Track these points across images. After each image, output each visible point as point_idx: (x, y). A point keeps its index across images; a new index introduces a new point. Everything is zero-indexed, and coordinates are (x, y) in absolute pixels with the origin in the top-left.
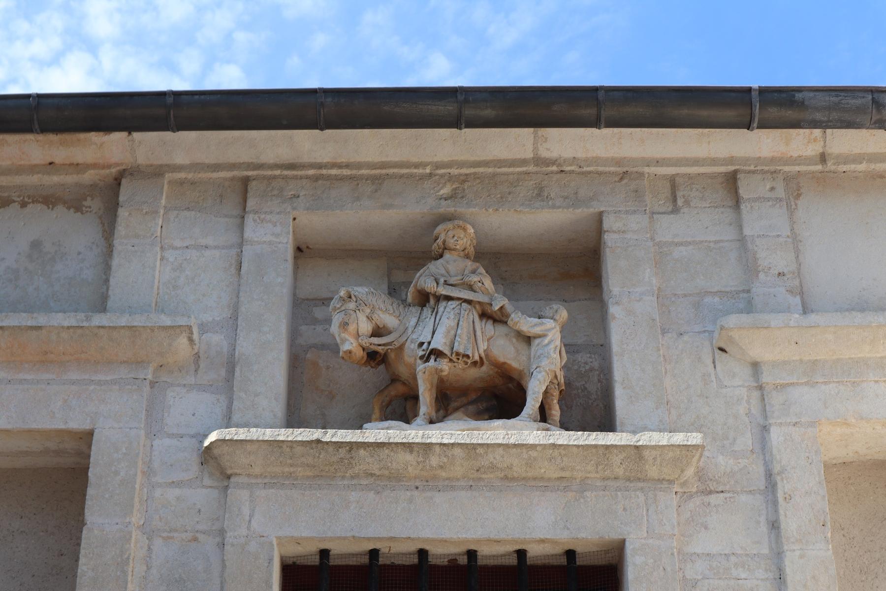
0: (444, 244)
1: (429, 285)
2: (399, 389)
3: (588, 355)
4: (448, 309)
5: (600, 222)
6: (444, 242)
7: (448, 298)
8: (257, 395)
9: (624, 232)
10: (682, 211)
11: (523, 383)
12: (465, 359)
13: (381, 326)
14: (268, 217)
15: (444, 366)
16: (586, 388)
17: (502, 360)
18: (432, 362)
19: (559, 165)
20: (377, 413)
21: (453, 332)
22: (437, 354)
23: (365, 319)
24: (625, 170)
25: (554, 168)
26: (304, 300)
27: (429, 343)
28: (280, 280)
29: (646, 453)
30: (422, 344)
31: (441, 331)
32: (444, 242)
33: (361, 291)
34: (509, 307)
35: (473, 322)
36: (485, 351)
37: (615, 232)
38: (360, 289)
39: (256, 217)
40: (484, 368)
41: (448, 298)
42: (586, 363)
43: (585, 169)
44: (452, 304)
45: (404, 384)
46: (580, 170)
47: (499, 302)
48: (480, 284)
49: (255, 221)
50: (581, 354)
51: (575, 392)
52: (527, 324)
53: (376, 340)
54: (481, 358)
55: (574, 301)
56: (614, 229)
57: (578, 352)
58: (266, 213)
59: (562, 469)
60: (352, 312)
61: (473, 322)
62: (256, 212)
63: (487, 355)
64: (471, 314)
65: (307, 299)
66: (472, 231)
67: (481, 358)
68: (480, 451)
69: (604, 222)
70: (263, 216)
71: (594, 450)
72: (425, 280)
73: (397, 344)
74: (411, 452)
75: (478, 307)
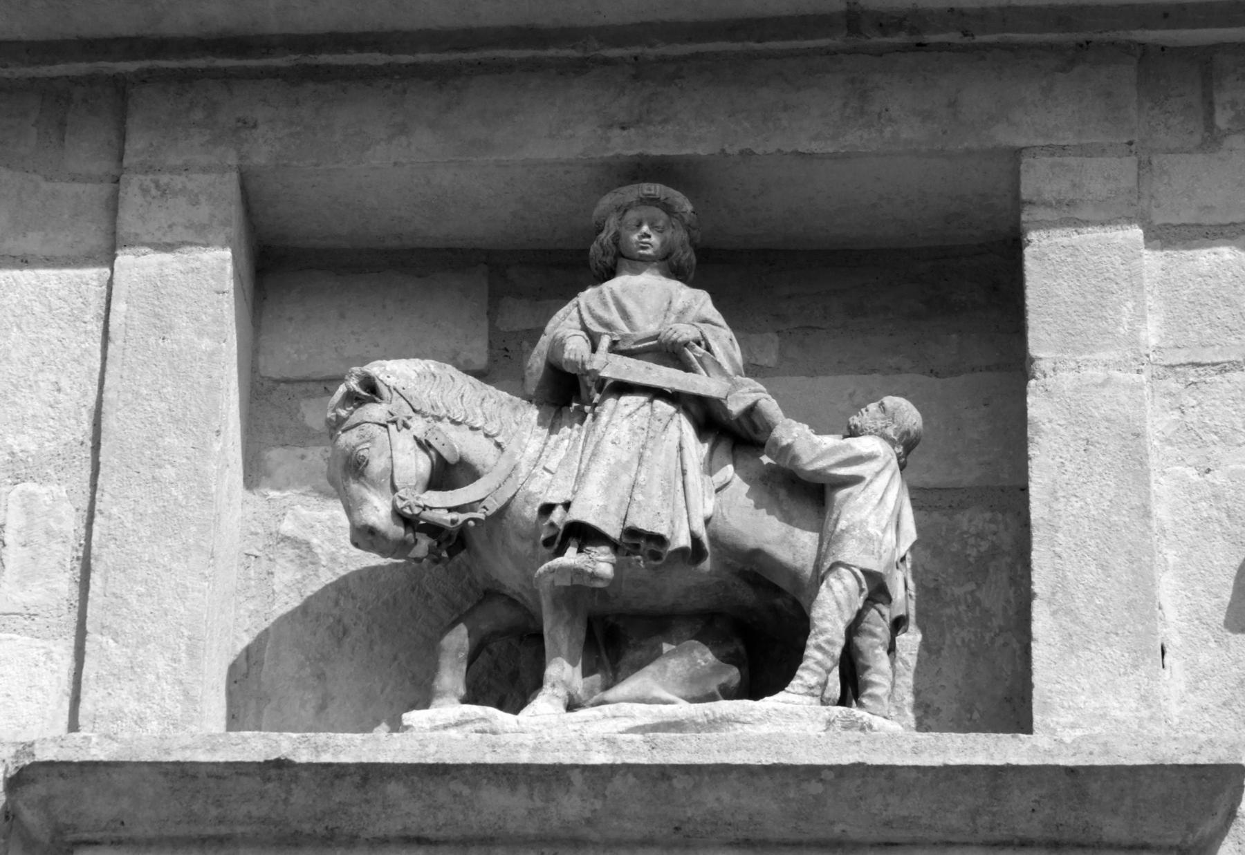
0: (616, 244)
1: (576, 347)
2: (501, 615)
3: (988, 515)
4: (617, 419)
5: (1016, 175)
6: (617, 236)
7: (622, 388)
8: (144, 642)
9: (1071, 204)
10: (1227, 143)
11: (802, 600)
12: (653, 546)
13: (451, 459)
14: (178, 181)
15: (601, 562)
16: (977, 602)
17: (751, 543)
18: (571, 558)
19: (913, 31)
20: (451, 677)
21: (626, 480)
22: (583, 534)
23: (412, 444)
24: (1081, 37)
25: (901, 38)
26: (278, 381)
27: (567, 505)
28: (206, 344)
29: (1094, 787)
30: (547, 509)
31: (598, 474)
32: (617, 236)
33: (394, 372)
34: (771, 406)
35: (681, 448)
36: (707, 521)
37: (1046, 204)
38: (393, 365)
39: (147, 180)
40: (707, 565)
41: (622, 388)
42: (980, 536)
43: (979, 38)
44: (630, 402)
45: (512, 602)
46: (966, 40)
47: (741, 395)
48: (701, 350)
49: (145, 191)
50: (968, 513)
51: (950, 611)
52: (813, 447)
53: (436, 498)
54: (695, 540)
55: (959, 373)
56: (1046, 196)
57: (962, 506)
58: (173, 170)
59: (888, 824)
60: (376, 430)
61: (681, 448)
62: (148, 169)
63: (713, 539)
64: (673, 428)
65: (287, 381)
66: (689, 207)
67: (695, 540)
68: (679, 783)
69: (1024, 180)
70: (164, 179)
71: (965, 779)
72: (566, 330)
73: (493, 506)
74: (513, 788)
75: (693, 408)
